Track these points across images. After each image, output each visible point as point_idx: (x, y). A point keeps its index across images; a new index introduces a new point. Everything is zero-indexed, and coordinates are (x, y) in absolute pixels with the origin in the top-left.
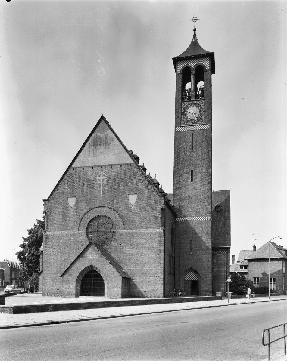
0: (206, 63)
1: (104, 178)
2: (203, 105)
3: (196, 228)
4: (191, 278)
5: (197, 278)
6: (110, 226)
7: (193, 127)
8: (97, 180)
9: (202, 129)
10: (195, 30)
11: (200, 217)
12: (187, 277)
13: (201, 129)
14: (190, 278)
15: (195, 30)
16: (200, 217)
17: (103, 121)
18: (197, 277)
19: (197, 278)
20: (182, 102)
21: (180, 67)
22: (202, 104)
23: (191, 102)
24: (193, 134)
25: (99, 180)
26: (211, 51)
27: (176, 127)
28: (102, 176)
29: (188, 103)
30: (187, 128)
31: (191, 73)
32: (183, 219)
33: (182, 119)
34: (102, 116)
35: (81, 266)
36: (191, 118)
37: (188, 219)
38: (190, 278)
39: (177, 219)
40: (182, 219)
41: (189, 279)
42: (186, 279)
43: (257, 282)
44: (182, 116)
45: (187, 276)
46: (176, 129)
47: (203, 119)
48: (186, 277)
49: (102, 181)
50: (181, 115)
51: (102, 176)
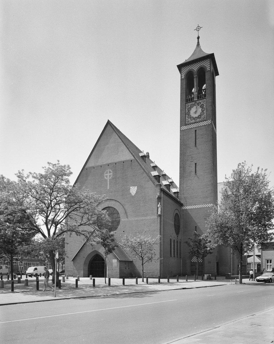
0: (207, 64)
1: (110, 174)
2: (204, 104)
3: (193, 215)
4: (195, 261)
5: (202, 261)
6: (116, 215)
7: (196, 124)
8: (105, 177)
9: (204, 125)
10: (198, 38)
11: (204, 205)
12: (193, 260)
13: (204, 125)
14: (194, 261)
15: (198, 38)
16: (204, 205)
17: (109, 125)
18: (202, 260)
19: (202, 261)
20: (186, 103)
21: (185, 70)
22: (204, 102)
23: (193, 103)
24: (196, 131)
25: (107, 176)
26: (210, 52)
27: (181, 126)
28: (108, 173)
29: (191, 104)
30: (202, 123)
31: (193, 76)
32: (205, 206)
33: (187, 118)
34: (108, 121)
35: (88, 251)
36: (194, 117)
37: (188, 208)
38: (194, 261)
39: (183, 208)
40: (206, 206)
41: (195, 261)
42: (200, 262)
43: (268, 265)
44: (187, 116)
45: (193, 259)
46: (182, 128)
47: (205, 115)
48: (192, 260)
49: (108, 177)
50: (186, 115)
51: (108, 173)
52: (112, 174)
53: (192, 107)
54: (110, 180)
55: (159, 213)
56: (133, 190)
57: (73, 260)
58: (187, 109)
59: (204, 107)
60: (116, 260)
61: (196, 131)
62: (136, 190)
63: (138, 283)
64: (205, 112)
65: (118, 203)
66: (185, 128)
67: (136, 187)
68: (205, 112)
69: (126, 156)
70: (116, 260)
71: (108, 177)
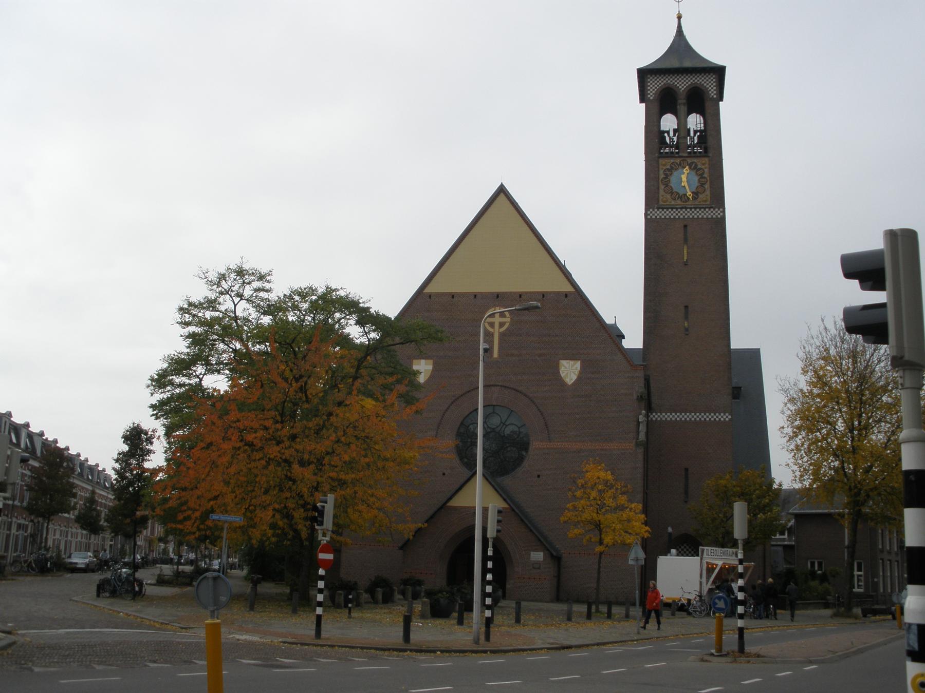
10: (679, 17)
15: (679, 17)
22: (704, 164)
24: (685, 226)
49: (497, 326)
52: (508, 320)
53: (676, 169)
54: (502, 335)
55: (642, 436)
56: (570, 371)
57: (401, 548)
58: (661, 172)
59: (705, 175)
60: (542, 554)
61: (685, 226)
62: (577, 372)
63: (412, 636)
64: (707, 186)
65: (493, 388)
66: (658, 214)
67: (578, 365)
68: (707, 186)
69: (570, 289)
70: (542, 554)
71: (497, 326)
